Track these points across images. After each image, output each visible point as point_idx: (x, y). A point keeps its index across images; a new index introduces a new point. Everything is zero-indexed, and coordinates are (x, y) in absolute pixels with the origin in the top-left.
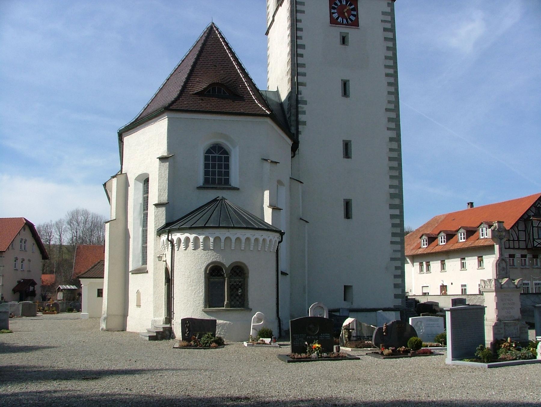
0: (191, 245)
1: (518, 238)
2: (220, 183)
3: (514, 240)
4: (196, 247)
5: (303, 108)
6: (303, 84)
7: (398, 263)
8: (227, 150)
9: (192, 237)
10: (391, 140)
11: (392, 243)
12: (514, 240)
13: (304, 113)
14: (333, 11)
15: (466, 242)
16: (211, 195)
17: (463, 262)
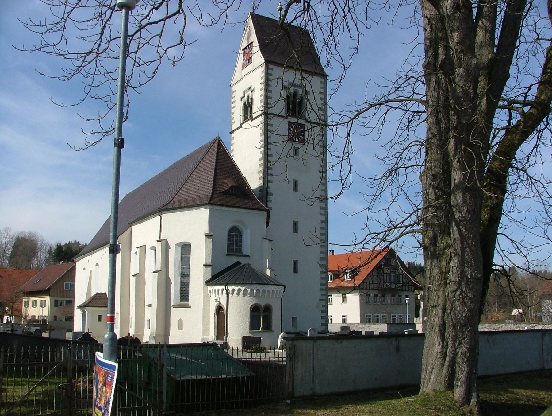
0: (242, 293)
1: (373, 282)
2: (236, 251)
3: (369, 283)
4: (245, 295)
5: (270, 198)
6: (271, 182)
7: (324, 303)
8: (241, 230)
9: (243, 289)
10: (322, 221)
11: (321, 289)
12: (369, 283)
13: (271, 201)
14: (290, 132)
15: (332, 282)
16: (234, 260)
17: (330, 298)
